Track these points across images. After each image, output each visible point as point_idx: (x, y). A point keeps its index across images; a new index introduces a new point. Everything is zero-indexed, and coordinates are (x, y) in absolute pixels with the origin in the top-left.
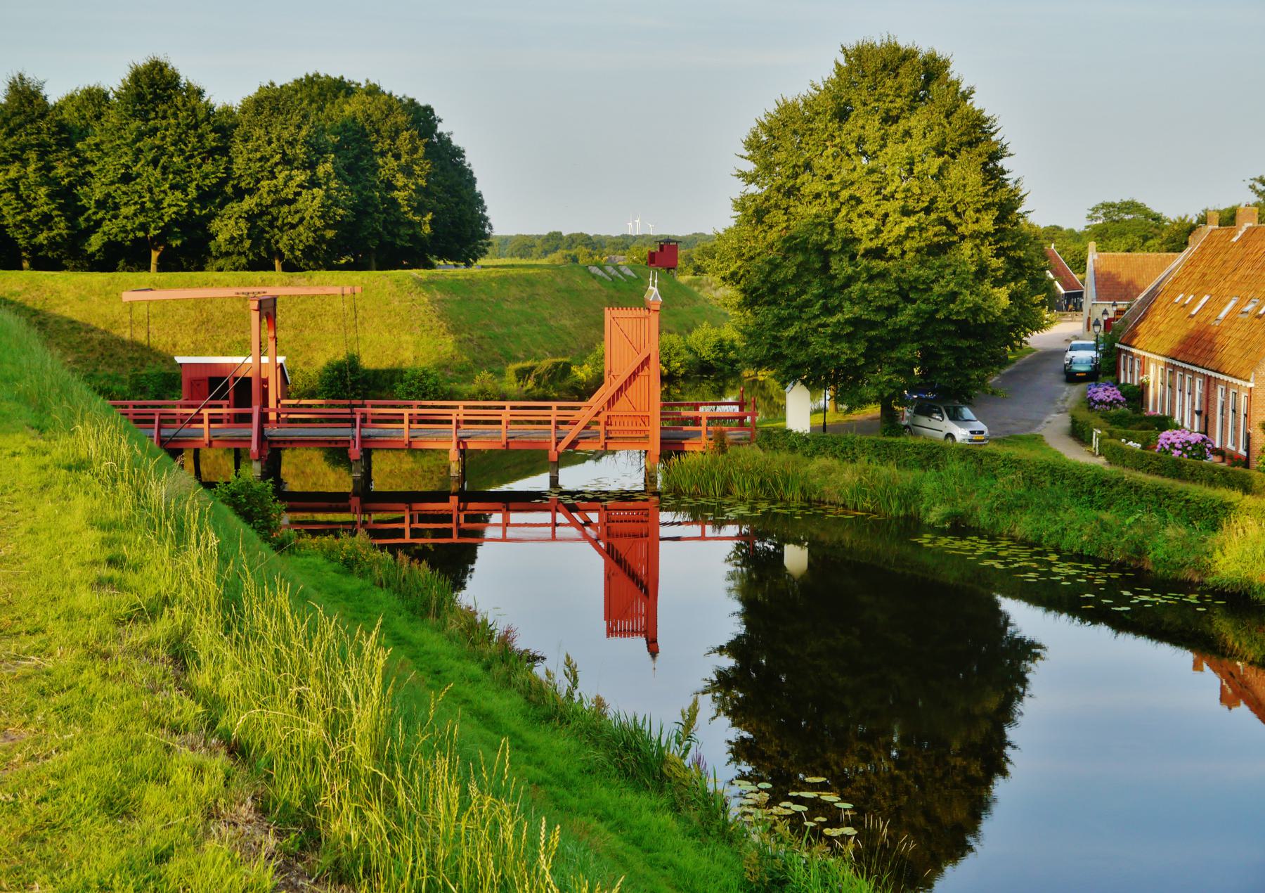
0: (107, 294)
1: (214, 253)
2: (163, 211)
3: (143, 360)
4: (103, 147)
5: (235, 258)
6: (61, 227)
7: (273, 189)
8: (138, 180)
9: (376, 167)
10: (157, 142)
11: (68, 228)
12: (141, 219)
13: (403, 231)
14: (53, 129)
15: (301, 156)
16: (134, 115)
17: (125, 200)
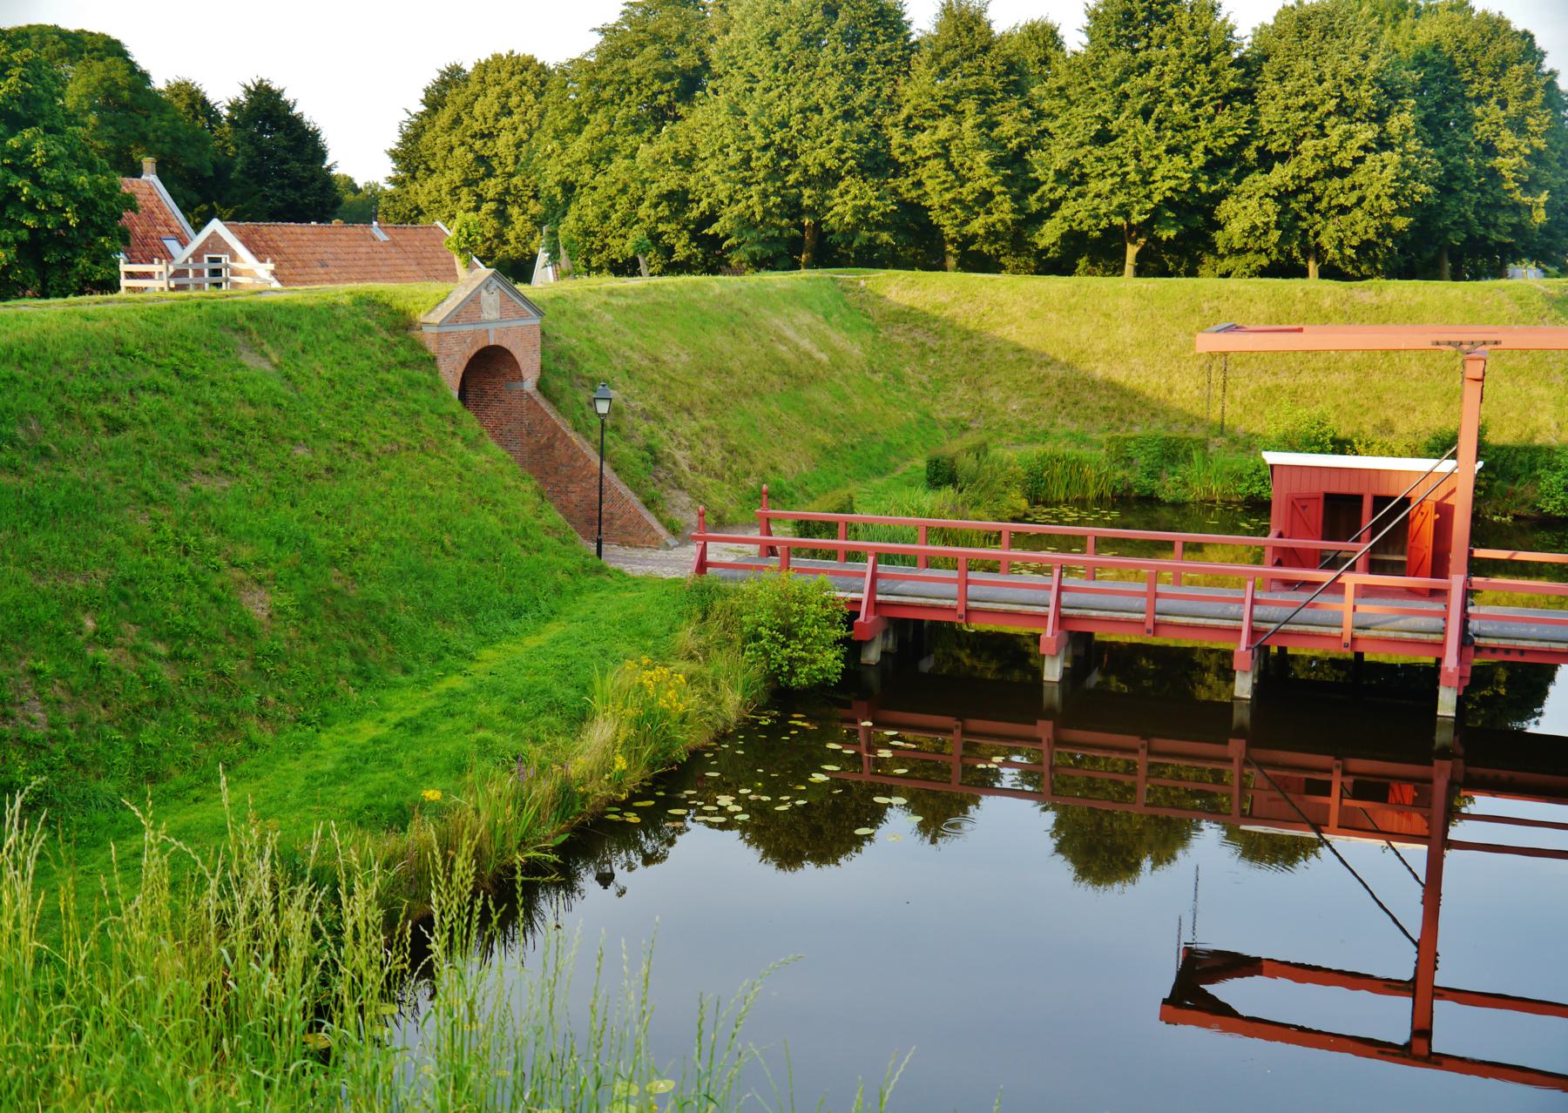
0: (1071, 309)
1: (1221, 250)
2: (1152, 186)
3: (1122, 412)
4: (1070, 91)
5: (1250, 257)
6: (1004, 211)
7: (1321, 153)
8: (1120, 140)
9: (1467, 122)
10: (1151, 83)
11: (1014, 211)
12: (1120, 198)
13: (1503, 218)
14: (1000, 68)
15: (1369, 101)
16: (1116, 45)
17: (1099, 170)
